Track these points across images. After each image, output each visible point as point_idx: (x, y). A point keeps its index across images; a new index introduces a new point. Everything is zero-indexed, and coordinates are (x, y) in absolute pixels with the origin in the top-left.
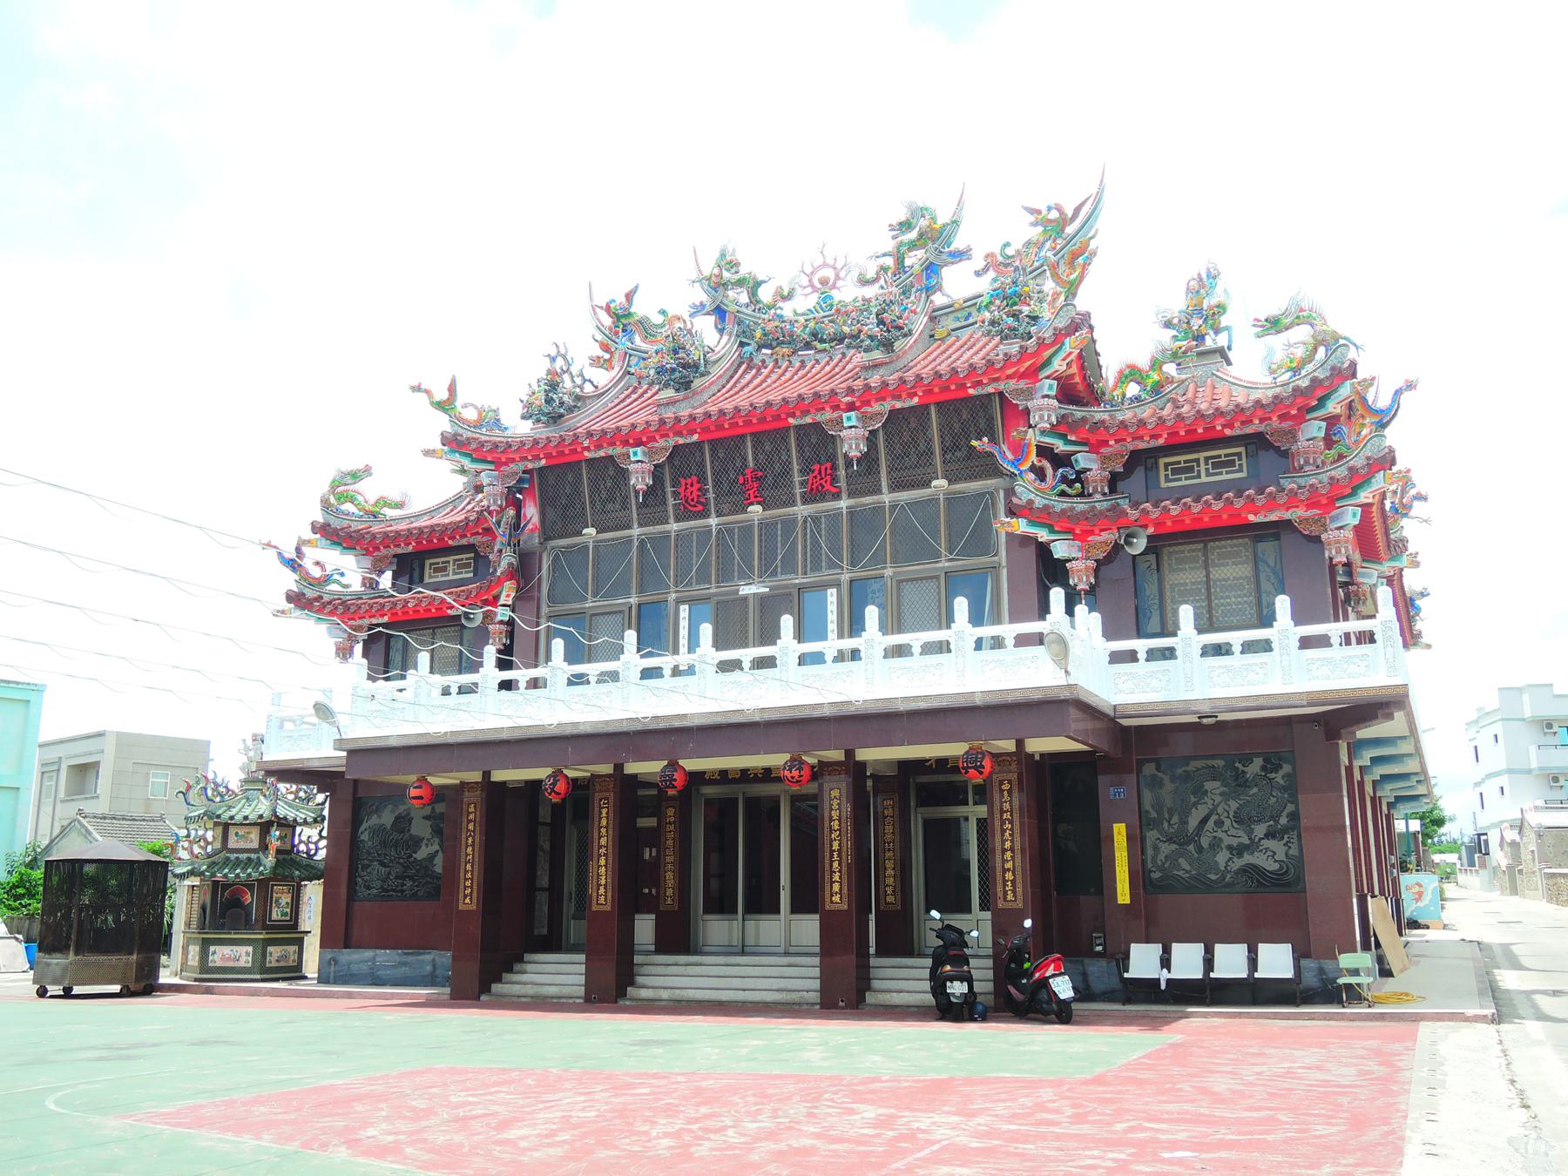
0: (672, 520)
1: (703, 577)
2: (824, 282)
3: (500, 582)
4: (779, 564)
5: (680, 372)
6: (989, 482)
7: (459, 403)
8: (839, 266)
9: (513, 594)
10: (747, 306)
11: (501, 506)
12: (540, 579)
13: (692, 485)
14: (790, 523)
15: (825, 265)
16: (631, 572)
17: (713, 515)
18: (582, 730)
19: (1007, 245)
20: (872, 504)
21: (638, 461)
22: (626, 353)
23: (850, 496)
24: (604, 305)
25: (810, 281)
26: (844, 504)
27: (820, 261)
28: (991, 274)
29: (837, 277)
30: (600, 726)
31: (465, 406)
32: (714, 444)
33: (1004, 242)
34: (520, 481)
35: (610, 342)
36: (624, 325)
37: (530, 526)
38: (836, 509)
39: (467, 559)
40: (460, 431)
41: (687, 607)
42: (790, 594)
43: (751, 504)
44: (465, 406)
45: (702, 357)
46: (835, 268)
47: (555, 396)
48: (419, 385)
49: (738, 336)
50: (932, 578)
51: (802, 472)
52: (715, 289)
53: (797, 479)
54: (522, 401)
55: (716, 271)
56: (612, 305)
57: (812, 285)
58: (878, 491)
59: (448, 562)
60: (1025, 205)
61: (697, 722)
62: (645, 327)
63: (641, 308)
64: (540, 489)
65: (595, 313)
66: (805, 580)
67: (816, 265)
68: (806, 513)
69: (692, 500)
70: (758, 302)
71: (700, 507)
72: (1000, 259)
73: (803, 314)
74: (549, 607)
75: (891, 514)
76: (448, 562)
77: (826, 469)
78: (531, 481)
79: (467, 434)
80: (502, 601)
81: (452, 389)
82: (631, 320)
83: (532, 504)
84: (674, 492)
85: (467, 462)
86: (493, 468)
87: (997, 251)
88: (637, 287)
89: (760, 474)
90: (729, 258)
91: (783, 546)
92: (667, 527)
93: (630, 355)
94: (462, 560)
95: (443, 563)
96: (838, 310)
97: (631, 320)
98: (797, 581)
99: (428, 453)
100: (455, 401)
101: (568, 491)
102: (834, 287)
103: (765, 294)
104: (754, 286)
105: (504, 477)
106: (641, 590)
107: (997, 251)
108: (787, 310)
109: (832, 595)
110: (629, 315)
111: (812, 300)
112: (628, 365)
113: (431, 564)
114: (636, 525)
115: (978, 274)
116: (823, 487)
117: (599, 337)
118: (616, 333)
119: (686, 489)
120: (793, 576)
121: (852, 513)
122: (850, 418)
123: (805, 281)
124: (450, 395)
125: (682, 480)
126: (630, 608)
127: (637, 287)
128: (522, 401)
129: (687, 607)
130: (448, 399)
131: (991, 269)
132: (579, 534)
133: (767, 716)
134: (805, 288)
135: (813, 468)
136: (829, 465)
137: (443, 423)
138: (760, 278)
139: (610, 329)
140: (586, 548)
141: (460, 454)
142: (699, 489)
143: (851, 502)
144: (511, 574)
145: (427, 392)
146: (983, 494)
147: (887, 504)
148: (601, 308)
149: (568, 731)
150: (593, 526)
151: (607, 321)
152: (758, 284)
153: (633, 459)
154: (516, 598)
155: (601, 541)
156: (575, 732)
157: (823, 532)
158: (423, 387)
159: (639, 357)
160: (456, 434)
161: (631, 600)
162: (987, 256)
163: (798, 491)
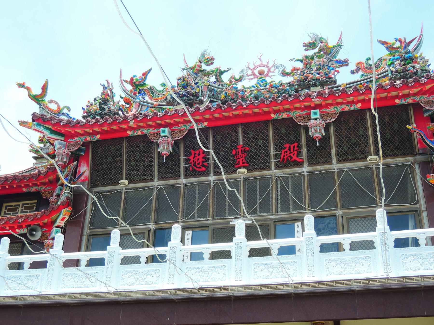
0: (182, 176)
1: (203, 212)
2: (261, 73)
3: (59, 209)
4: (259, 206)
5: (188, 97)
6: (407, 158)
7: (47, 99)
8: (270, 65)
9: (67, 218)
10: (215, 83)
11: (65, 163)
12: (85, 211)
13: (199, 155)
14: (266, 181)
15: (262, 65)
16: (151, 209)
17: (212, 174)
18: (134, 297)
19: (369, 59)
20: (324, 170)
21: (165, 137)
22: (140, 104)
23: (309, 164)
24: (129, 80)
25: (253, 72)
26: (305, 169)
27: (259, 63)
28: (360, 73)
29: (269, 71)
30: (150, 294)
31: (51, 102)
32: (215, 129)
33: (367, 57)
34: (79, 150)
35: (131, 98)
36: (140, 90)
37: (82, 178)
38: (299, 173)
39: (31, 204)
40: (46, 114)
41: (190, 232)
42: (268, 225)
43: (240, 168)
44: (51, 102)
45: (200, 91)
46: (268, 67)
47: (105, 107)
48: (24, 83)
49: (209, 97)
50: (368, 217)
51: (276, 149)
52: (196, 74)
53: (272, 153)
54: (83, 109)
55: (198, 64)
56: (135, 78)
57: (254, 74)
58: (330, 162)
59: (19, 205)
60: (380, 39)
61: (237, 293)
62: (152, 91)
63: (150, 82)
64: (93, 155)
65: (122, 84)
66: (278, 217)
67: (256, 65)
68: (278, 175)
69: (198, 164)
70: (222, 81)
71: (204, 169)
72: (365, 65)
73: (249, 88)
74: (90, 229)
75: (339, 178)
76: (19, 205)
77: (294, 147)
78: (87, 152)
79: (48, 116)
80: (57, 224)
81: (45, 88)
82: (144, 88)
83: (85, 165)
84: (185, 159)
85: (47, 134)
86: (63, 139)
87: (364, 61)
88: (150, 70)
89: (247, 149)
90: (207, 57)
91: (261, 196)
92: (178, 181)
93: (142, 105)
94: (28, 204)
95: (15, 206)
96: (271, 86)
97: (144, 88)
98: (272, 217)
99: (23, 123)
100: (45, 96)
101: (109, 159)
102: (267, 75)
103: (225, 78)
104: (219, 74)
105: (68, 146)
106: (157, 220)
107: (364, 61)
108: (239, 86)
109: (298, 226)
110: (144, 84)
111: (254, 82)
112: (141, 110)
113: (6, 207)
114: (156, 179)
115: (353, 72)
116: (291, 158)
117: (124, 95)
118: (135, 94)
119: (195, 157)
120: (269, 214)
121: (310, 175)
122: (315, 114)
123: (250, 72)
124: (43, 92)
125: (193, 152)
126: (149, 231)
127: (150, 70)
128: (83, 109)
129: (190, 232)
130: (41, 94)
131: (361, 70)
132: (117, 183)
133: (299, 289)
134: (250, 75)
135: (285, 146)
136: (296, 144)
137: (35, 108)
138: (222, 70)
139: (131, 92)
140: (121, 192)
141: (44, 127)
142: (203, 158)
143: (310, 168)
144: (67, 204)
145: (28, 89)
146: (404, 166)
147: (336, 170)
148: (126, 82)
149: (123, 297)
150: (126, 179)
151: (129, 87)
152: (222, 73)
153: (162, 134)
154: (68, 223)
155: (131, 189)
156: (128, 298)
157: (290, 187)
158: (26, 85)
159: (148, 107)
160: (42, 115)
161: (150, 226)
162: (358, 64)
163: (273, 160)
